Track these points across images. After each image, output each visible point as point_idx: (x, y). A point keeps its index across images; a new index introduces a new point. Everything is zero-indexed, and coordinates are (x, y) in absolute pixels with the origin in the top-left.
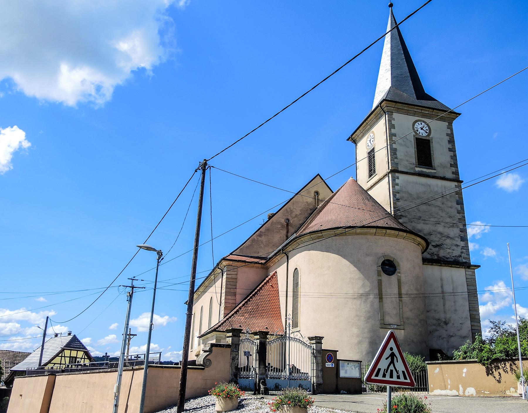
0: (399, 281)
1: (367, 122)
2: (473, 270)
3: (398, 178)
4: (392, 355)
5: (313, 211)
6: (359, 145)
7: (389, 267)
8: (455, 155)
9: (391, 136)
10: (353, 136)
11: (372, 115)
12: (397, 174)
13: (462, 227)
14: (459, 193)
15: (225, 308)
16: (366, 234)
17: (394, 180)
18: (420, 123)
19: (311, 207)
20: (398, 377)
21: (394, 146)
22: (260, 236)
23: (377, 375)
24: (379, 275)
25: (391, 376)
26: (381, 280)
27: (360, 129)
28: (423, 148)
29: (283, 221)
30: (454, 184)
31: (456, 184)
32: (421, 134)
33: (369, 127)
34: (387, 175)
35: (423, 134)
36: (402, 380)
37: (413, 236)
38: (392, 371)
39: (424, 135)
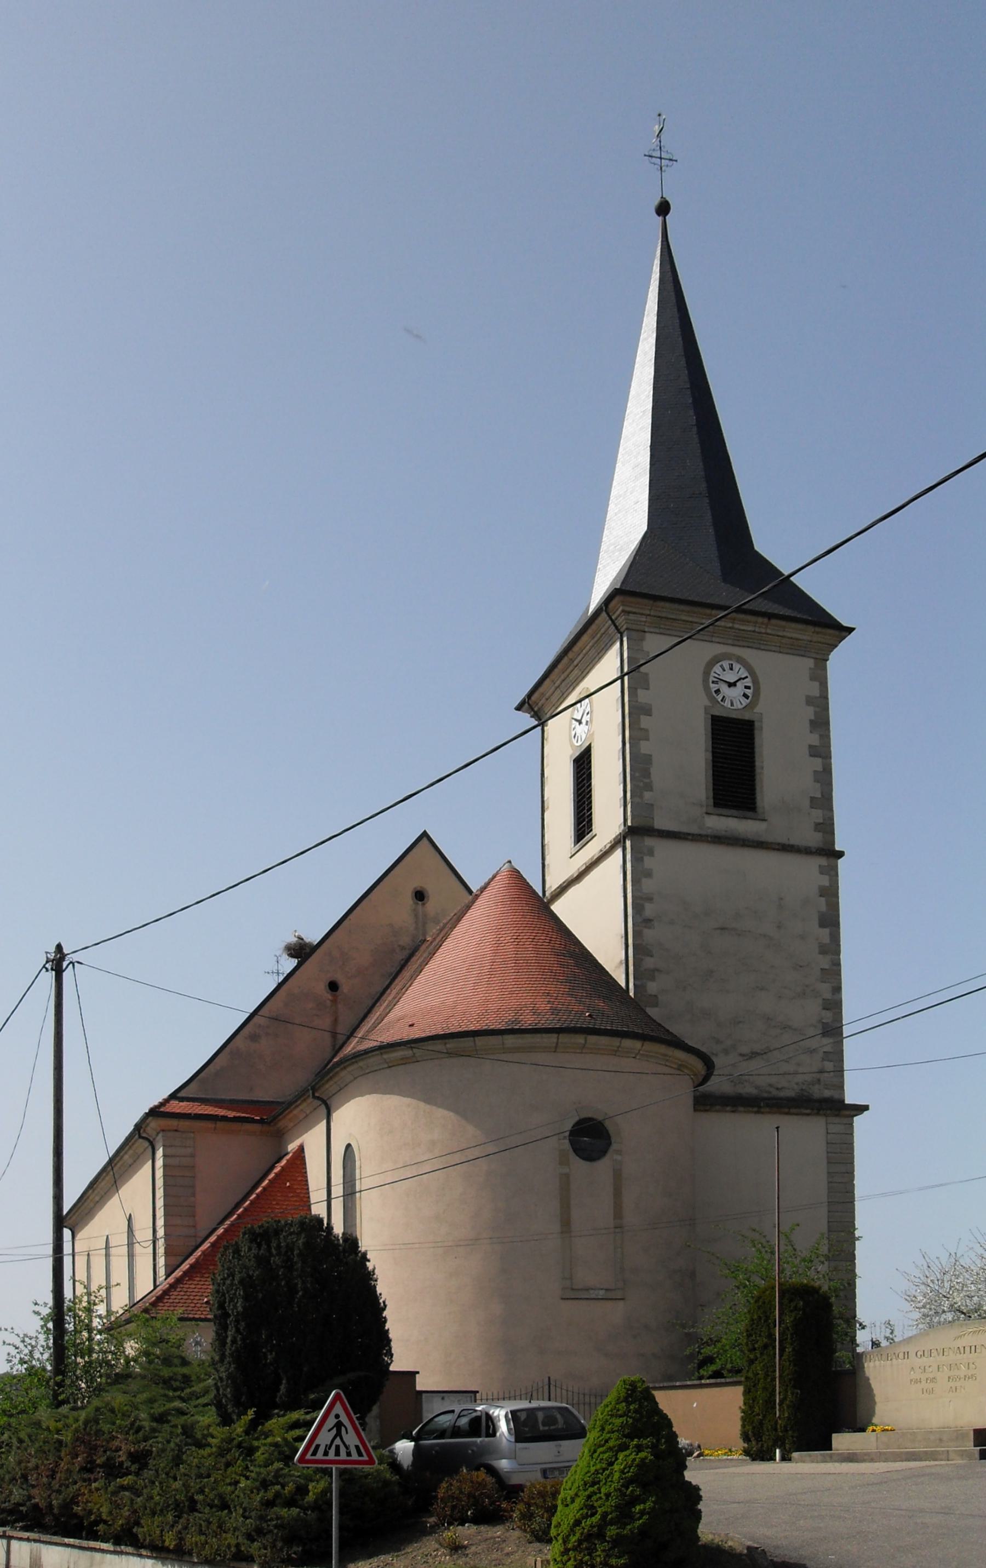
0: (618, 1175)
1: (570, 655)
2: (845, 1120)
3: (651, 853)
4: (339, 1425)
5: (404, 959)
6: (553, 725)
7: (590, 1137)
8: (827, 770)
9: (636, 716)
10: (533, 698)
11: (585, 638)
12: (649, 842)
13: (828, 996)
14: (830, 893)
15: (167, 1253)
16: (531, 1049)
17: (637, 860)
18: (726, 664)
19: (405, 940)
20: (349, 1454)
21: (645, 747)
22: (254, 1038)
23: (314, 1454)
24: (563, 1161)
25: (337, 1453)
26: (567, 1176)
27: (553, 676)
28: (733, 755)
29: (321, 988)
30: (815, 863)
31: (823, 861)
32: (727, 704)
33: (576, 672)
34: (618, 842)
35: (734, 700)
36: (355, 1456)
37: (662, 1049)
38: (338, 1447)
39: (738, 705)
